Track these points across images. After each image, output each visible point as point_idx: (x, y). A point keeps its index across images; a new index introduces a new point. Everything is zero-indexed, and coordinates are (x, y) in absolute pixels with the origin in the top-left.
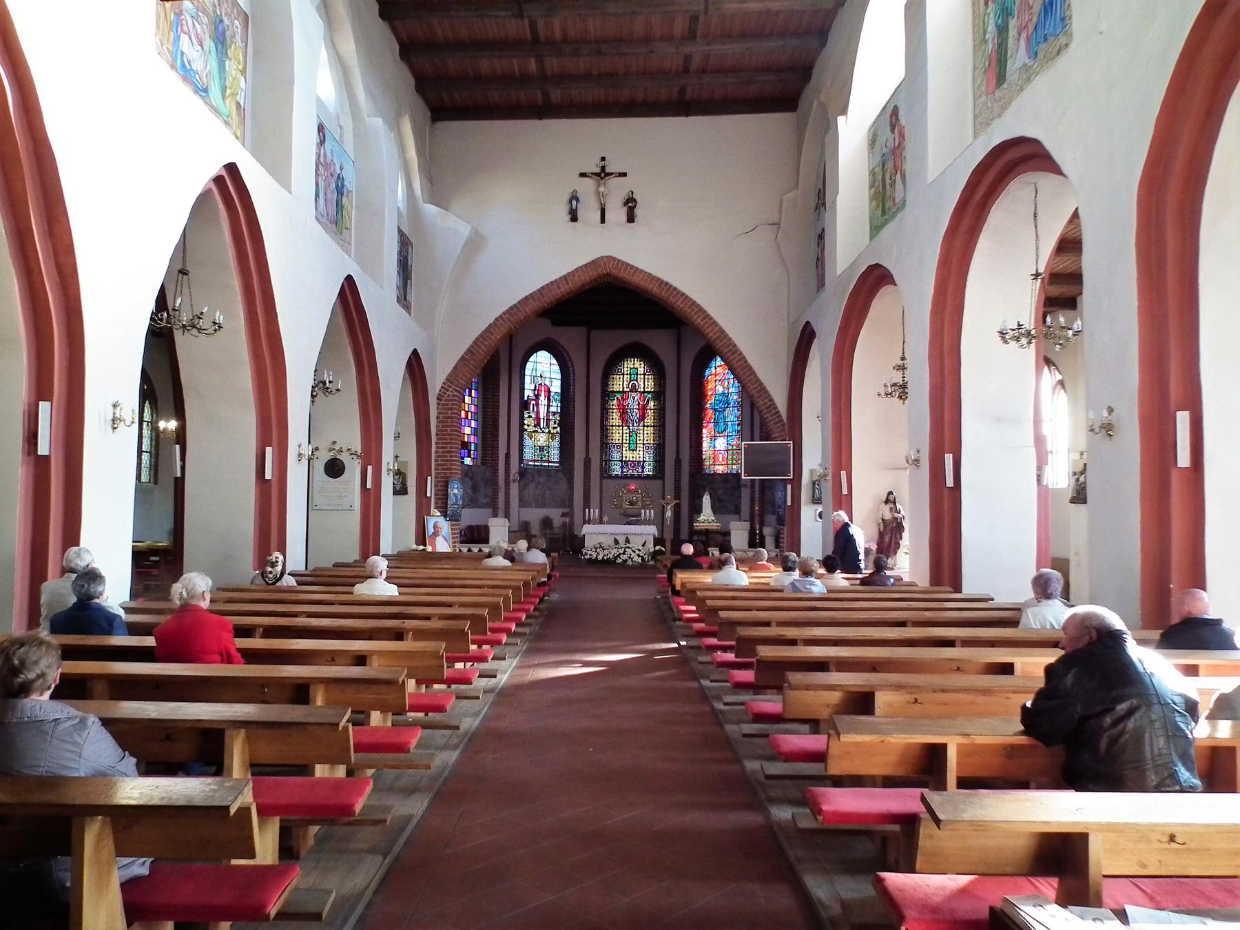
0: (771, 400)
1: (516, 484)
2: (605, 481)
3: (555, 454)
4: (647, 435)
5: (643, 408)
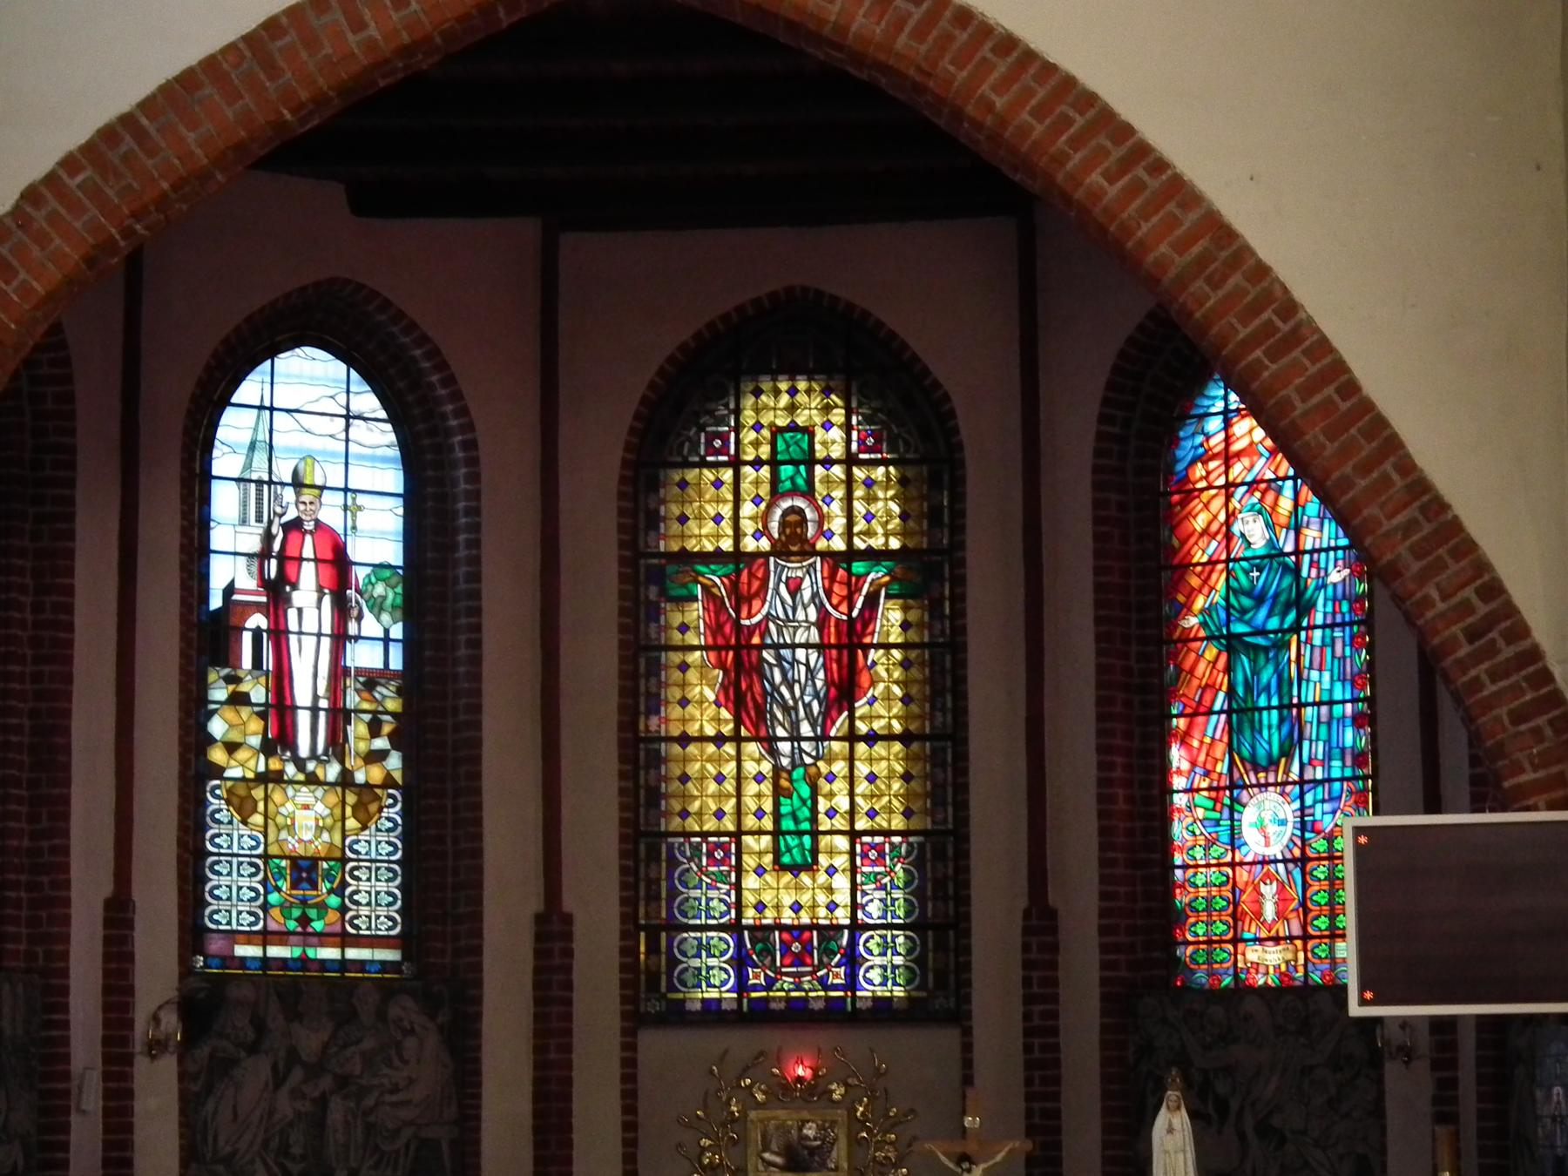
0: (1494, 590)
1: (168, 1065)
2: (652, 1042)
3: (376, 900)
4: (869, 783)
5: (846, 645)
